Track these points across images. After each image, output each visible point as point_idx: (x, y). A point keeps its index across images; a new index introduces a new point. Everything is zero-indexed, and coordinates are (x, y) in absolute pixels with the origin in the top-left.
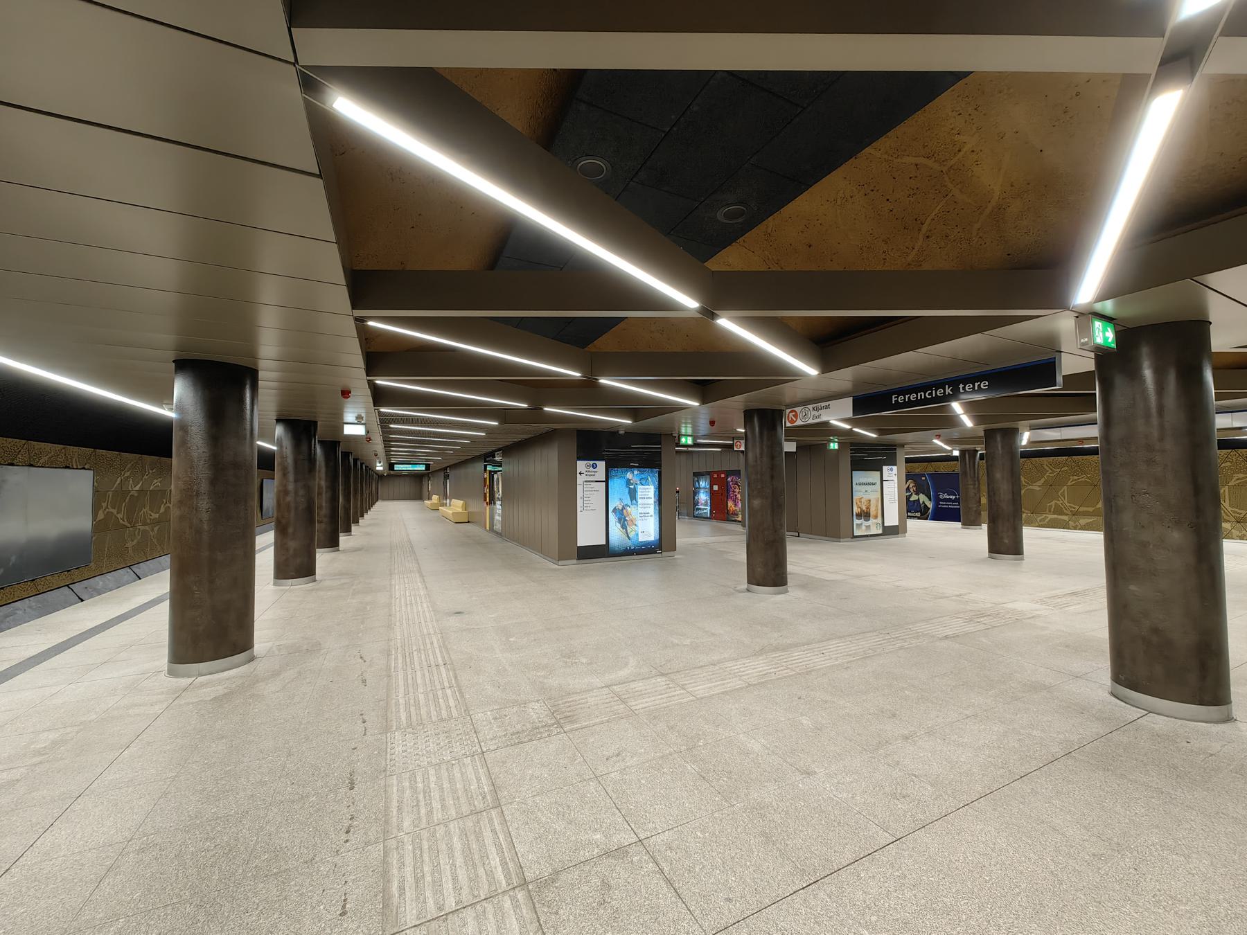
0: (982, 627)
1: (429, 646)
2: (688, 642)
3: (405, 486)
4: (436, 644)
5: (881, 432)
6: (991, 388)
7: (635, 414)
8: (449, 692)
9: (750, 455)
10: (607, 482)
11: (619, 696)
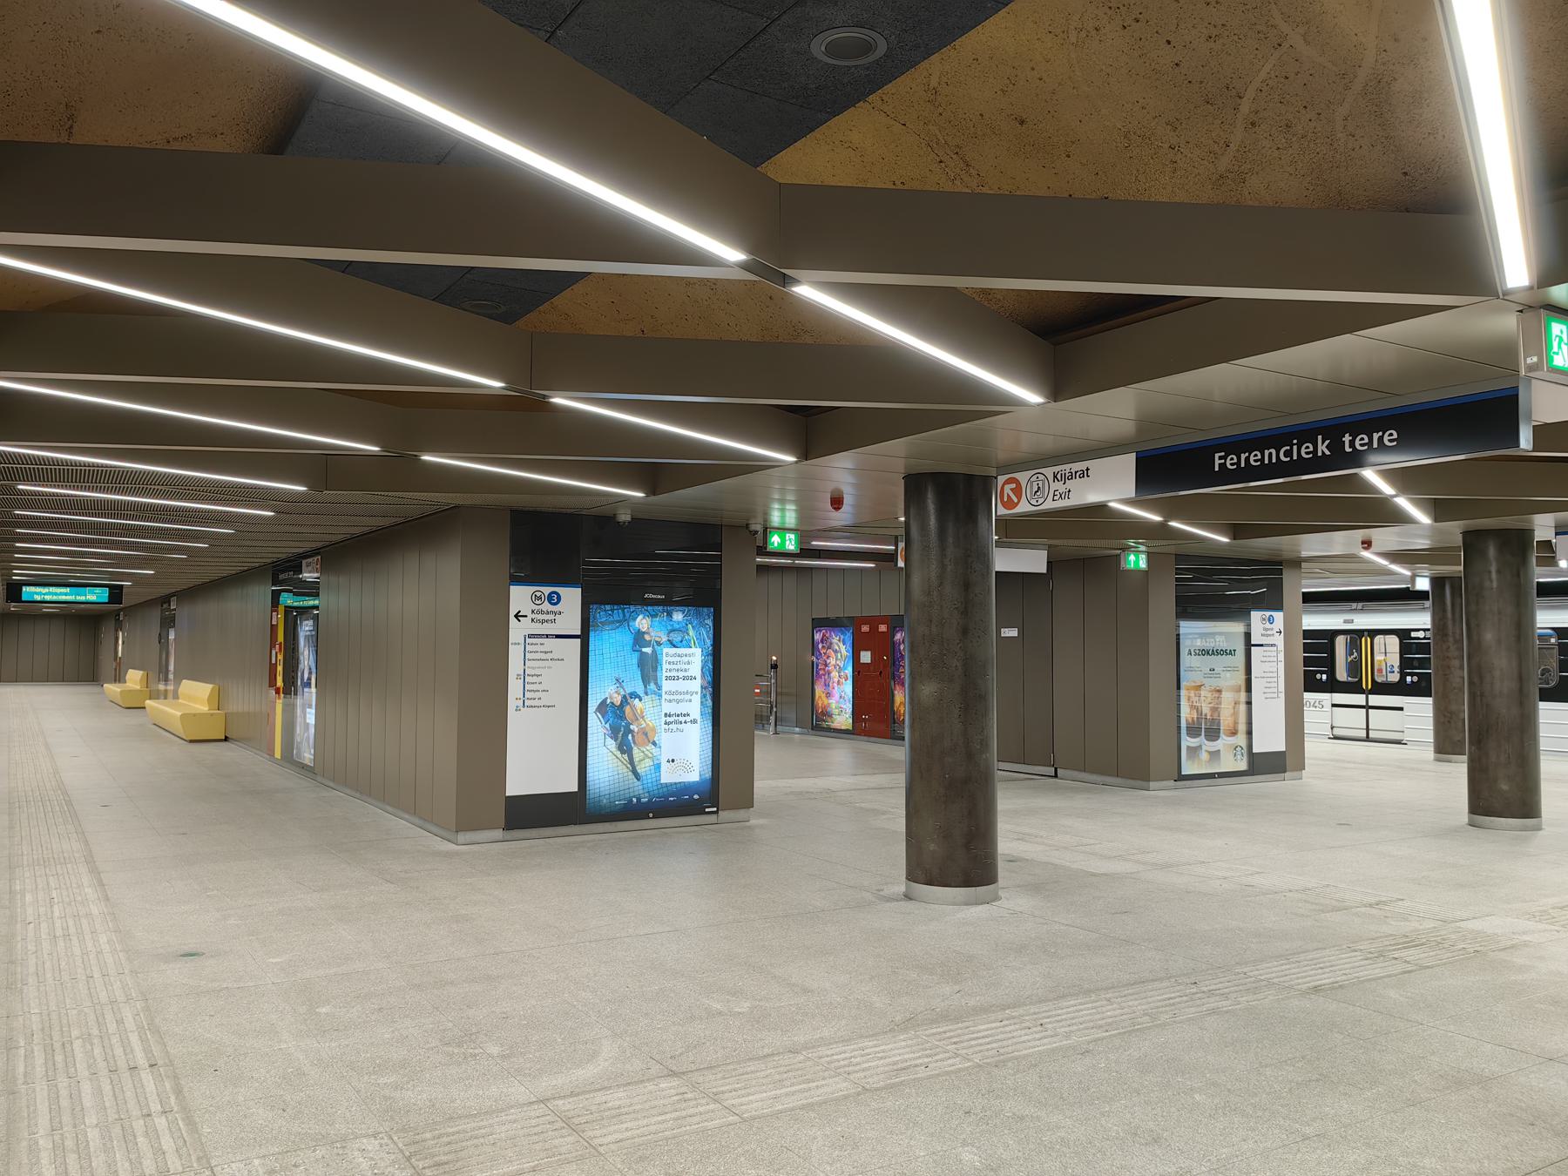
0: (1400, 967)
1: (112, 1027)
2: (744, 1007)
3: (51, 644)
4: (130, 1023)
5: (1236, 532)
6: (1403, 444)
7: (652, 477)
8: (161, 1122)
9: (916, 579)
10: (584, 638)
11: (567, 1121)
